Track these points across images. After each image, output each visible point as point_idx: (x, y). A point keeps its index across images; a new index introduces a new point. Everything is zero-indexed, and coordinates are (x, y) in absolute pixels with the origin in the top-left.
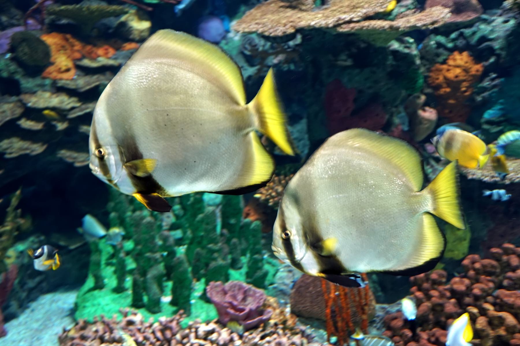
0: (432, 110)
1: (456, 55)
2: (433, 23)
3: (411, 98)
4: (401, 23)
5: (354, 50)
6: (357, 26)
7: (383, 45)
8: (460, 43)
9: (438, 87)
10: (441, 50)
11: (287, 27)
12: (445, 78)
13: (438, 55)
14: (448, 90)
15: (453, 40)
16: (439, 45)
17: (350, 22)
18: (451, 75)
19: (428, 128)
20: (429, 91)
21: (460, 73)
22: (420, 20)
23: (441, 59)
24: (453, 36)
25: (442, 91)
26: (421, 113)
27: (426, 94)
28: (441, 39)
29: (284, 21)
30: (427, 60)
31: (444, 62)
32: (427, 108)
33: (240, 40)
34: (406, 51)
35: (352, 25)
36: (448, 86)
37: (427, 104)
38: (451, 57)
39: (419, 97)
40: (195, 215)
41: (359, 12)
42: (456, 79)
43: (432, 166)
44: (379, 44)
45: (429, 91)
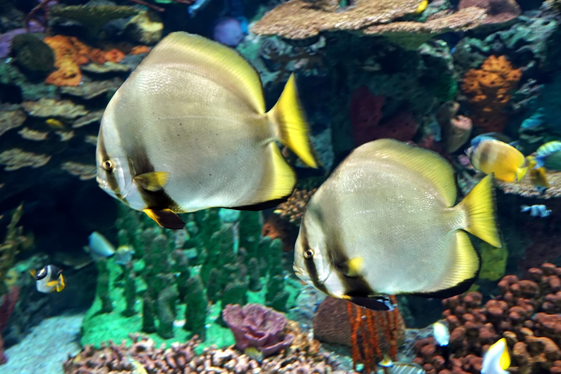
0: (466, 119)
1: (492, 60)
2: (467, 25)
3: (443, 105)
4: (433, 25)
5: (382, 54)
6: (385, 28)
7: (413, 49)
8: (497, 46)
9: (473, 94)
10: (476, 54)
11: (310, 29)
12: (481, 84)
13: (472, 60)
14: (483, 97)
15: (489, 43)
16: (474, 49)
17: (378, 23)
18: (486, 81)
19: (462, 139)
20: (462, 98)
21: (496, 79)
22: (453, 21)
23: (475, 64)
24: (489, 38)
25: (477, 98)
26: (454, 122)
27: (459, 102)
28: (476, 42)
29: (306, 23)
30: (461, 65)
31: (479, 67)
32: (461, 117)
33: (259, 43)
34: (439, 55)
35: (380, 27)
36: (484, 93)
37: (460, 112)
38: (486, 62)
39: (452, 105)
40: (210, 233)
41: (388, 13)
42: (491, 86)
43: (466, 180)
44: (408, 48)
45: (462, 98)
